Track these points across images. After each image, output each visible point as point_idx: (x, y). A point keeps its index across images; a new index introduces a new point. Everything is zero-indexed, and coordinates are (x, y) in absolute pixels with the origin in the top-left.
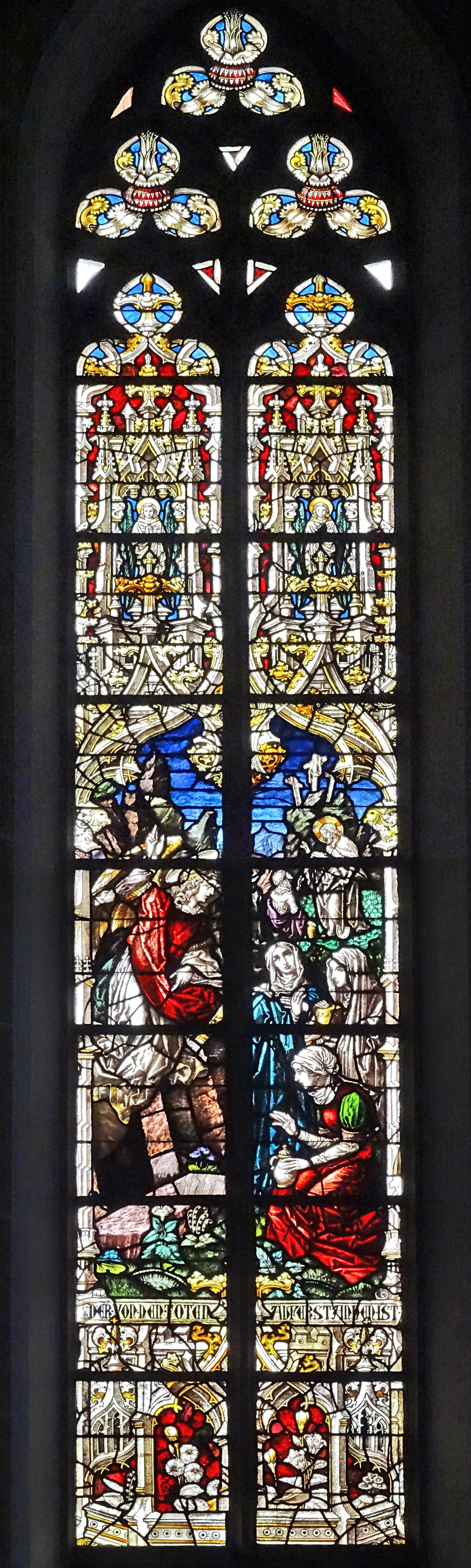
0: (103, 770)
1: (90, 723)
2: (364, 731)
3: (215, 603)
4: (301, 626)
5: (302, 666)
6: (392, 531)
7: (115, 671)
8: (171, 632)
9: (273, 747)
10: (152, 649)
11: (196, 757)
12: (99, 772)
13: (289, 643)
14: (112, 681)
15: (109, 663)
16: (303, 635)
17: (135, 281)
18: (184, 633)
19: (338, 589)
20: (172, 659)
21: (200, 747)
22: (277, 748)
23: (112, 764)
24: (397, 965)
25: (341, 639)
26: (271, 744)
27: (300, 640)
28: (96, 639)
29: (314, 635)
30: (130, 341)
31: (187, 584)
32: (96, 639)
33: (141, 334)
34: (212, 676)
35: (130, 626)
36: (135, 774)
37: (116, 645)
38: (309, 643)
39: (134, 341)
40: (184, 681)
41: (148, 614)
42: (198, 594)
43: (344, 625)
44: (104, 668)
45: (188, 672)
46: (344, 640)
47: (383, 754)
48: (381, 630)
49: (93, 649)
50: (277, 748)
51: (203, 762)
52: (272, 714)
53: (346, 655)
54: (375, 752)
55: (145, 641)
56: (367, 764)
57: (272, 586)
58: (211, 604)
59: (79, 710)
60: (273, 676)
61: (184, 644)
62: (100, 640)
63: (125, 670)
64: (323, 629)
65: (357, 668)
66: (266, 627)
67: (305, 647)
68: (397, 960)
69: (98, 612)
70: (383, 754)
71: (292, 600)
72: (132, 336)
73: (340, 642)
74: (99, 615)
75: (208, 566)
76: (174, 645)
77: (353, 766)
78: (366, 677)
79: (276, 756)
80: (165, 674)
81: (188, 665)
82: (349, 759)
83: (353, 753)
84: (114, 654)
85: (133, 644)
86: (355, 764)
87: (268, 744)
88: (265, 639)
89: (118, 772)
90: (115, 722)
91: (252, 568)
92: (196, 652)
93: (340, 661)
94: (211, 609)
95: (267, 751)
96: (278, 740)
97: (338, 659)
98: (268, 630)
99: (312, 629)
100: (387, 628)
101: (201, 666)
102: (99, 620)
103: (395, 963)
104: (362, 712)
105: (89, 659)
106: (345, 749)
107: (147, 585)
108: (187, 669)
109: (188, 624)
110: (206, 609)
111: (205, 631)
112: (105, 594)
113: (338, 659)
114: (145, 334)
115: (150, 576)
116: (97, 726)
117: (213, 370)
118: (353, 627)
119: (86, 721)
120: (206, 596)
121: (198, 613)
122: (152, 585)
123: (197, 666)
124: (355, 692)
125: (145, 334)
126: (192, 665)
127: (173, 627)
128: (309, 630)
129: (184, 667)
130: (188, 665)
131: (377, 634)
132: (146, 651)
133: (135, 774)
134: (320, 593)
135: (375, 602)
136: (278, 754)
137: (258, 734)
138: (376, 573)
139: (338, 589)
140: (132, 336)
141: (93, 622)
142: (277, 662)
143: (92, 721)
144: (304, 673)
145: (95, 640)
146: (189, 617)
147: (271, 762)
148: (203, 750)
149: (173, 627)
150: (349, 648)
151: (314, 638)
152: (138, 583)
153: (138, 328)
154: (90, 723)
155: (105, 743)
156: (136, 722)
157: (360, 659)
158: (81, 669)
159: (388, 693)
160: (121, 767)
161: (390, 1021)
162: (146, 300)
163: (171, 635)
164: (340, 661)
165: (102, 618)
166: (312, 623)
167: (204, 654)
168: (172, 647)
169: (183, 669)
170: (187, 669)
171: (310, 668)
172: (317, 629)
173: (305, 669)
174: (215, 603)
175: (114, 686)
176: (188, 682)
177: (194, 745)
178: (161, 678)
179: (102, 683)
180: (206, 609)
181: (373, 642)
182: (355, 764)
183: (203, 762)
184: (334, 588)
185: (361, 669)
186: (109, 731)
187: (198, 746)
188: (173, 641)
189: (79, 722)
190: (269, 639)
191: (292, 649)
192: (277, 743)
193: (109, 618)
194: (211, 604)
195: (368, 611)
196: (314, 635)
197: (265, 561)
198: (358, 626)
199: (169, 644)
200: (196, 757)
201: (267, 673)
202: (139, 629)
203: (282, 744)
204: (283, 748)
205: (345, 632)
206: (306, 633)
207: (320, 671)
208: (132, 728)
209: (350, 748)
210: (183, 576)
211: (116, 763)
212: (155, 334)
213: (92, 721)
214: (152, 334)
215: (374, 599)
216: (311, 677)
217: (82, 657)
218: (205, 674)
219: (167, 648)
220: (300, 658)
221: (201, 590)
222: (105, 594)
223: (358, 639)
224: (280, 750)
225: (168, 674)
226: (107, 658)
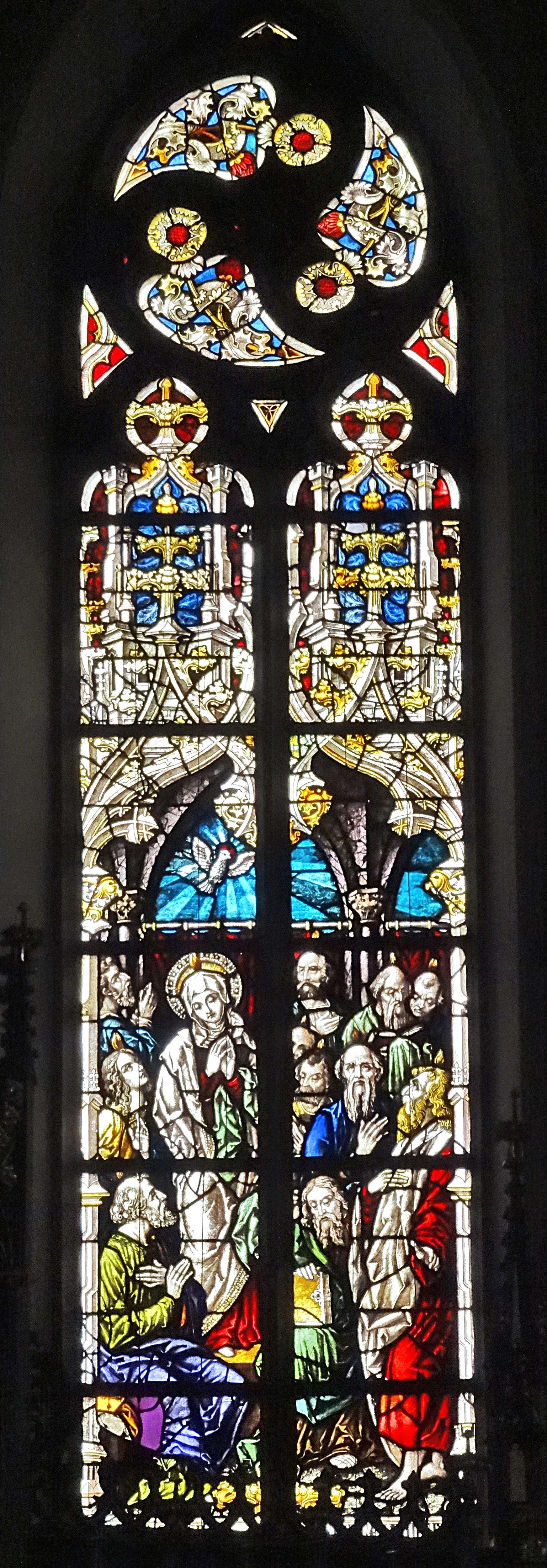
0: (113, 825)
1: (97, 765)
2: (425, 768)
3: (245, 604)
4: (348, 633)
5: (350, 686)
6: (348, 1527)
7: (127, 692)
8: (191, 641)
9: (316, 793)
10: (170, 663)
11: (225, 808)
12: (108, 828)
13: (333, 655)
14: (123, 706)
15: (119, 682)
16: (349, 644)
17: (152, 388)
18: (209, 643)
19: (394, 585)
20: (196, 676)
21: (230, 795)
22: (320, 794)
23: (124, 818)
24: (467, 1076)
25: (397, 651)
26: (314, 788)
27: (347, 652)
28: (104, 651)
29: (365, 644)
30: (146, 464)
31: (212, 579)
32: (104, 651)
33: (158, 457)
34: (242, 698)
35: (143, 633)
36: (151, 831)
37: (127, 658)
38: (358, 656)
39: (152, 465)
40: (210, 706)
41: (165, 617)
42: (226, 591)
43: (399, 631)
44: (114, 689)
45: (214, 693)
46: (400, 652)
47: (450, 799)
48: (444, 638)
49: (100, 664)
50: (320, 794)
51: (233, 815)
52: (314, 750)
53: (403, 671)
54: (439, 796)
55: (162, 653)
56: (429, 811)
57: (314, 579)
58: (241, 605)
59: (85, 746)
60: (315, 699)
61: (208, 657)
62: (107, 652)
63: (138, 692)
64: (375, 637)
65: (416, 689)
66: (305, 633)
67: (353, 660)
68: (467, 1070)
69: (104, 615)
70: (450, 799)
71: (338, 598)
72: (148, 458)
73: (395, 655)
74: (107, 620)
75: (237, 556)
76: (198, 658)
77: (412, 816)
78: (427, 699)
79: (318, 804)
80: (186, 699)
81: (213, 684)
82: (408, 806)
83: (412, 798)
84: (125, 669)
85: (146, 657)
86: (415, 812)
87: (311, 788)
88: (305, 651)
89: (130, 827)
90: (128, 763)
91: (292, 554)
92: (223, 666)
93: (396, 678)
94: (241, 611)
95: (310, 799)
96: (322, 783)
97: (393, 677)
98: (307, 639)
99: (361, 636)
100: (452, 635)
101: (229, 686)
102: (106, 625)
103: (464, 1073)
104: (423, 745)
105: (94, 677)
106: (403, 794)
107: (165, 580)
108: (212, 689)
109: (213, 632)
110: (235, 610)
111: (234, 641)
112: (114, 592)
113: (393, 677)
114: (164, 456)
115: (168, 568)
116: (106, 767)
117: (237, 829)
118: (410, 634)
119: (93, 761)
120: (235, 592)
121: (225, 617)
122: (170, 580)
123: (225, 686)
124: (413, 719)
125: (164, 456)
126: (219, 684)
127: (193, 634)
128: (357, 638)
129: (208, 688)
130: (213, 684)
131: (438, 643)
132: (163, 663)
133: (151, 831)
134: (372, 589)
135: (438, 601)
136: (322, 801)
137: (298, 776)
138: (440, 563)
139: (394, 585)
140: (148, 458)
141: (99, 629)
142: (319, 681)
143: (100, 762)
144: (352, 694)
145: (101, 653)
146: (213, 621)
147: (313, 812)
148: (231, 800)
149: (193, 634)
150: (407, 662)
151: (364, 649)
152: (154, 577)
153: (154, 449)
154: (97, 765)
155: (116, 790)
156: (152, 763)
157: (420, 676)
158: (86, 692)
159: (454, 720)
160: (134, 821)
161: (458, 1151)
162: (163, 412)
163: (192, 646)
164: (396, 678)
165: (111, 623)
166: (360, 630)
167: (232, 670)
168: (195, 661)
169: (207, 690)
170: (212, 689)
171: (359, 688)
172: (368, 637)
173: (354, 691)
174: (245, 604)
175: (126, 713)
176: (214, 706)
177: (223, 792)
178: (181, 702)
179: (110, 709)
180: (235, 610)
181: (436, 655)
182: (415, 812)
183: (233, 815)
184: (388, 583)
185: (421, 690)
186: (120, 774)
187: (227, 794)
188: (194, 654)
189: (85, 763)
190: (311, 651)
191: (339, 662)
192: (320, 787)
193: (118, 622)
194: (241, 605)
195: (429, 612)
196: (365, 644)
197: (306, 545)
198: (417, 633)
199: (190, 656)
200: (225, 808)
201: (308, 695)
202: (154, 637)
203: (327, 788)
204: (328, 793)
205: (402, 640)
206: (353, 641)
207: (372, 692)
208: (148, 771)
209: (409, 792)
210: (207, 568)
211: (129, 816)
212: (176, 456)
213: (100, 762)
214: (172, 456)
215: (437, 598)
216: (361, 699)
217: (88, 677)
218: (235, 696)
219: (189, 662)
220: (345, 675)
221: (229, 585)
222: (114, 592)
223: (416, 651)
224: (325, 796)
225: (190, 697)
226: (117, 676)
